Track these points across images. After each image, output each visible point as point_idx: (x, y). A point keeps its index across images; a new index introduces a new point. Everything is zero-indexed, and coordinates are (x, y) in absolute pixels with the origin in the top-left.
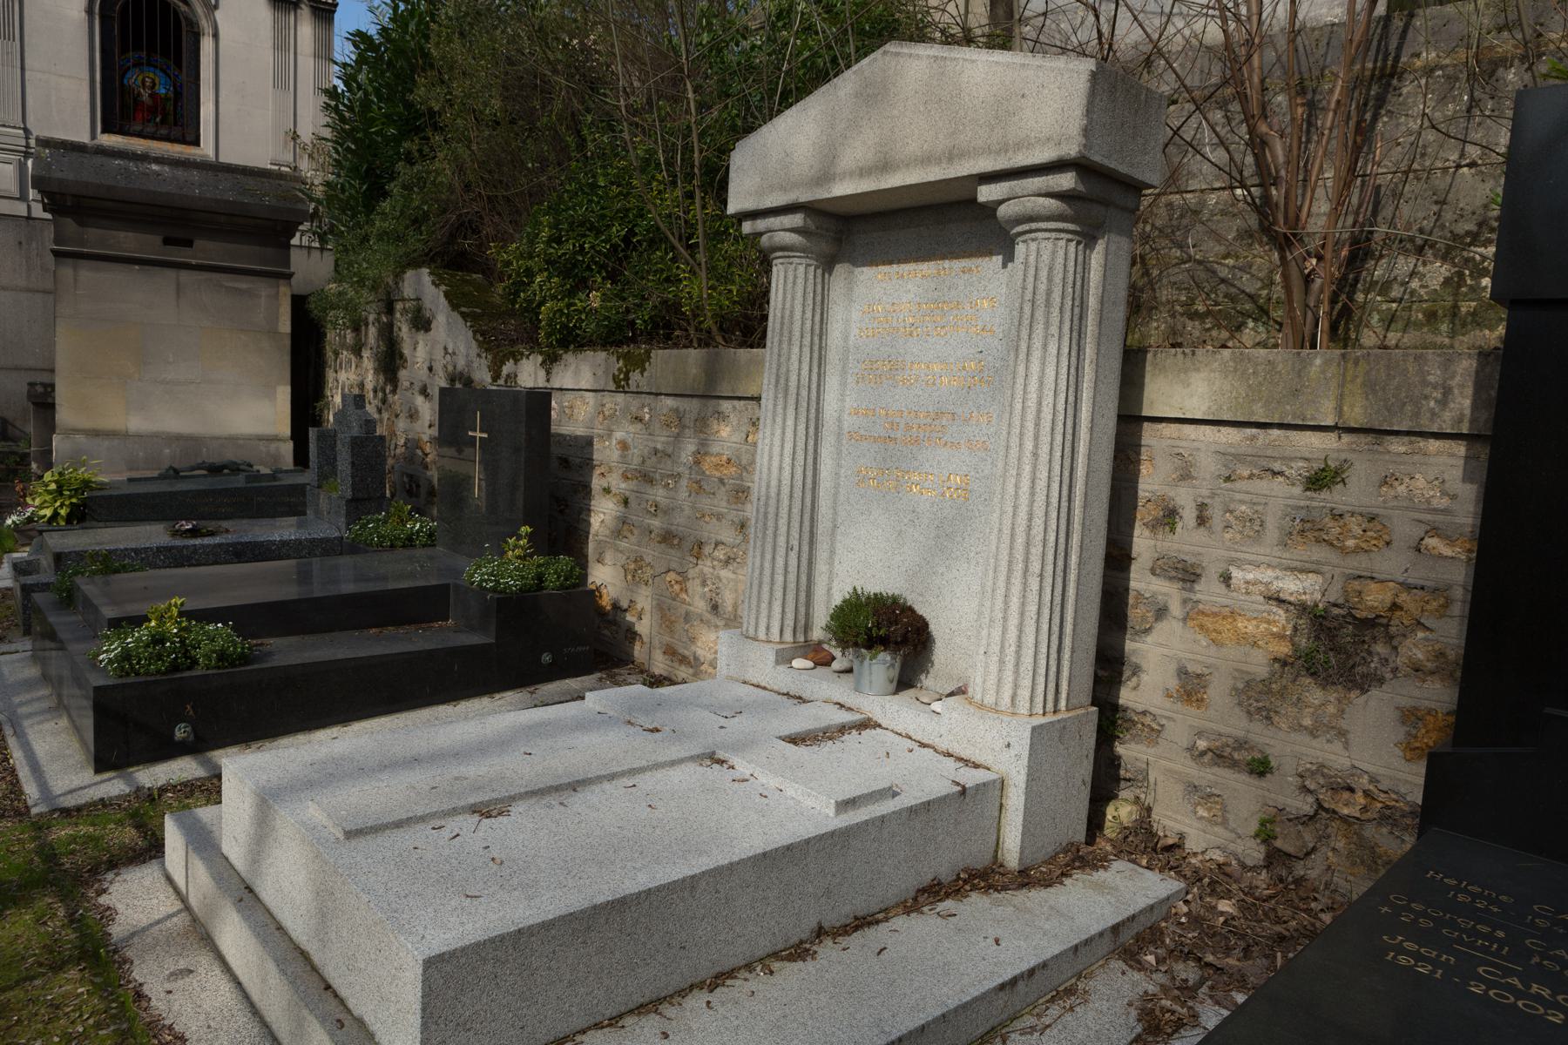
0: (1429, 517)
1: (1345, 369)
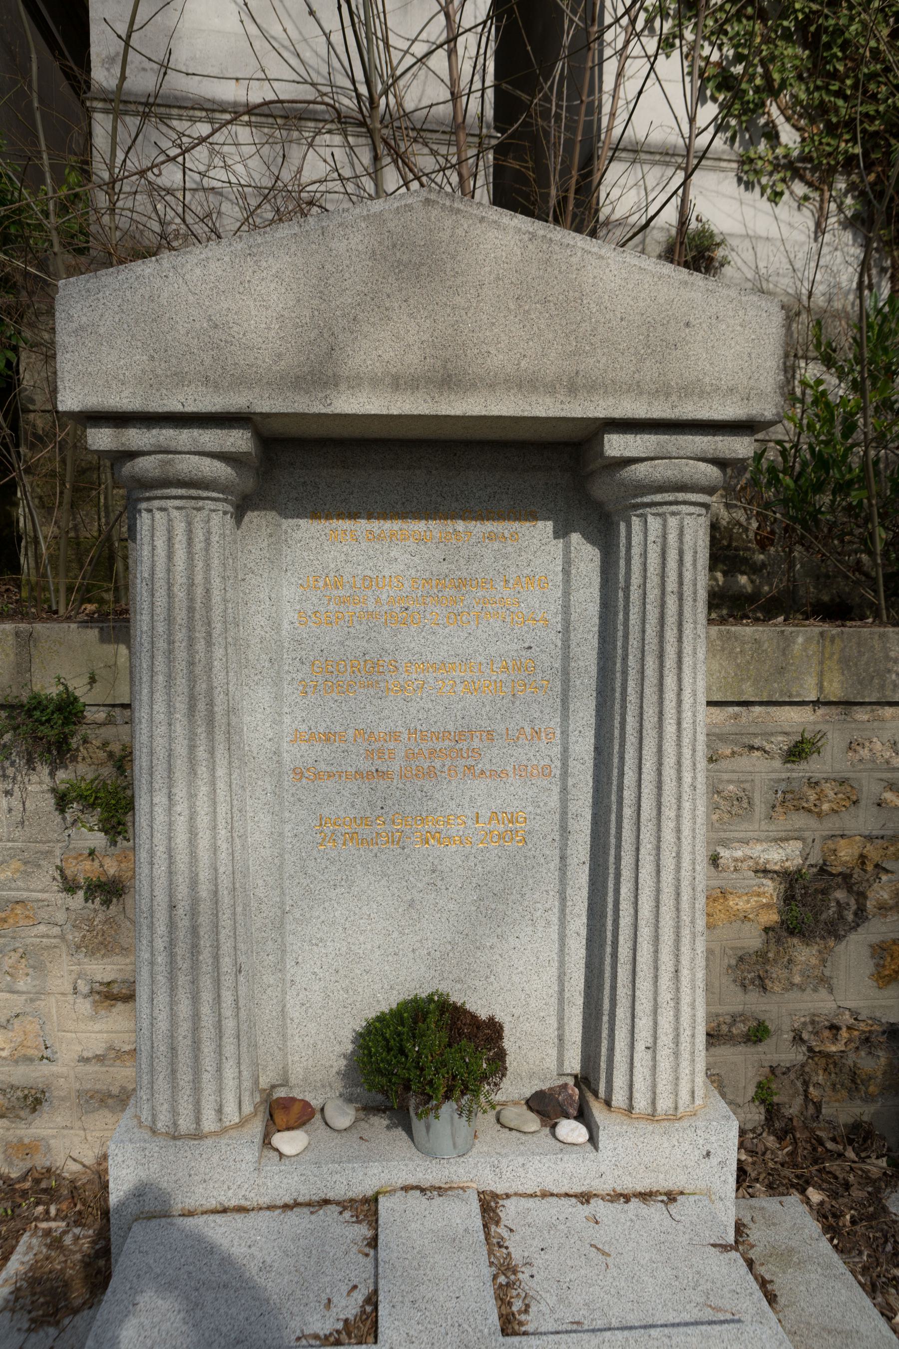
0: (889, 775)
1: (824, 646)
